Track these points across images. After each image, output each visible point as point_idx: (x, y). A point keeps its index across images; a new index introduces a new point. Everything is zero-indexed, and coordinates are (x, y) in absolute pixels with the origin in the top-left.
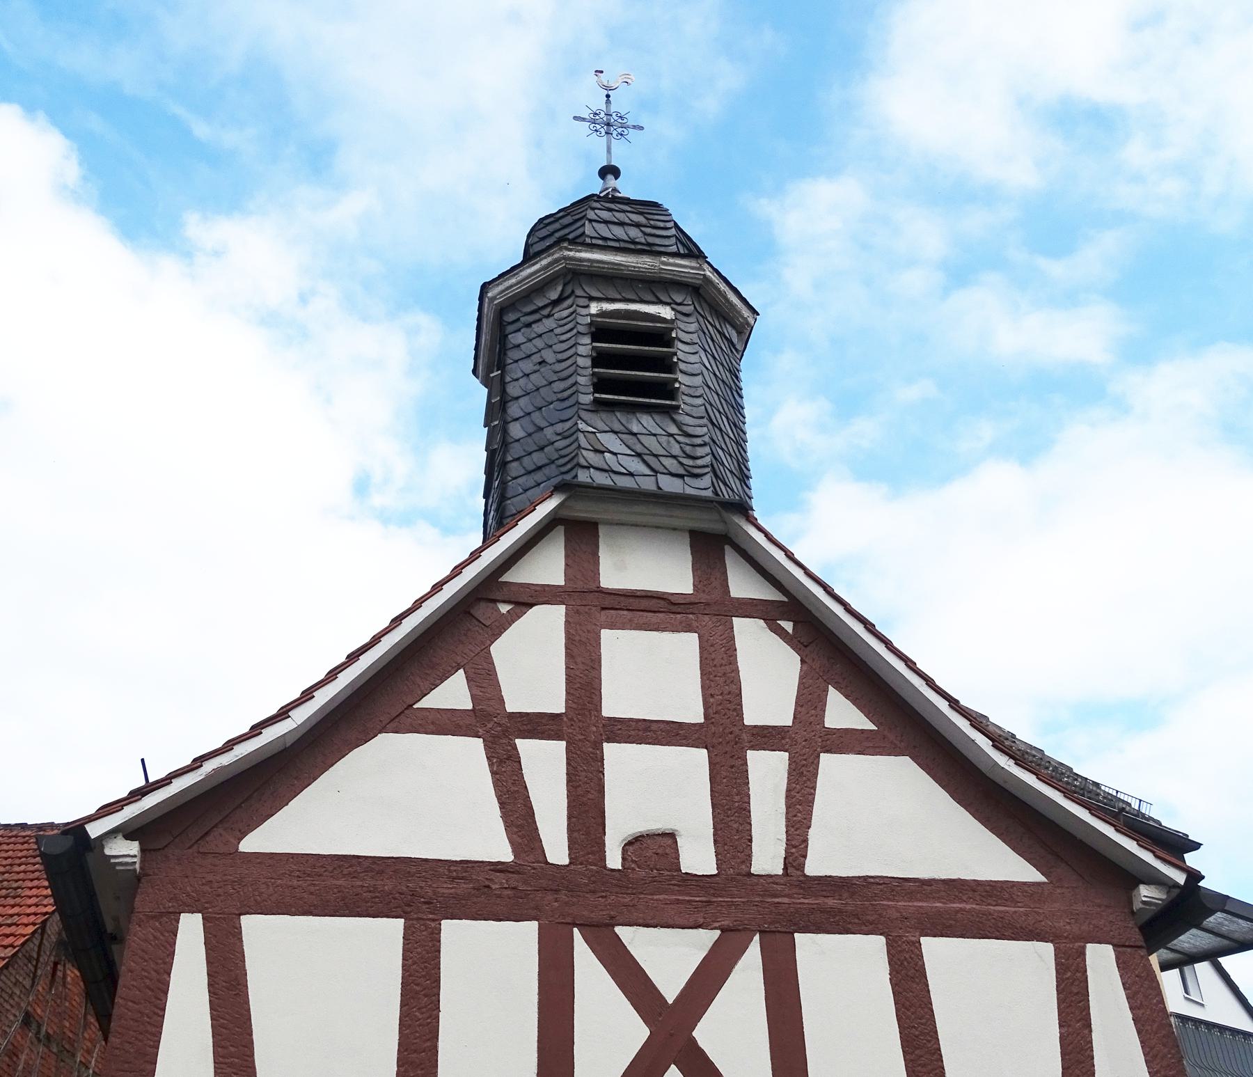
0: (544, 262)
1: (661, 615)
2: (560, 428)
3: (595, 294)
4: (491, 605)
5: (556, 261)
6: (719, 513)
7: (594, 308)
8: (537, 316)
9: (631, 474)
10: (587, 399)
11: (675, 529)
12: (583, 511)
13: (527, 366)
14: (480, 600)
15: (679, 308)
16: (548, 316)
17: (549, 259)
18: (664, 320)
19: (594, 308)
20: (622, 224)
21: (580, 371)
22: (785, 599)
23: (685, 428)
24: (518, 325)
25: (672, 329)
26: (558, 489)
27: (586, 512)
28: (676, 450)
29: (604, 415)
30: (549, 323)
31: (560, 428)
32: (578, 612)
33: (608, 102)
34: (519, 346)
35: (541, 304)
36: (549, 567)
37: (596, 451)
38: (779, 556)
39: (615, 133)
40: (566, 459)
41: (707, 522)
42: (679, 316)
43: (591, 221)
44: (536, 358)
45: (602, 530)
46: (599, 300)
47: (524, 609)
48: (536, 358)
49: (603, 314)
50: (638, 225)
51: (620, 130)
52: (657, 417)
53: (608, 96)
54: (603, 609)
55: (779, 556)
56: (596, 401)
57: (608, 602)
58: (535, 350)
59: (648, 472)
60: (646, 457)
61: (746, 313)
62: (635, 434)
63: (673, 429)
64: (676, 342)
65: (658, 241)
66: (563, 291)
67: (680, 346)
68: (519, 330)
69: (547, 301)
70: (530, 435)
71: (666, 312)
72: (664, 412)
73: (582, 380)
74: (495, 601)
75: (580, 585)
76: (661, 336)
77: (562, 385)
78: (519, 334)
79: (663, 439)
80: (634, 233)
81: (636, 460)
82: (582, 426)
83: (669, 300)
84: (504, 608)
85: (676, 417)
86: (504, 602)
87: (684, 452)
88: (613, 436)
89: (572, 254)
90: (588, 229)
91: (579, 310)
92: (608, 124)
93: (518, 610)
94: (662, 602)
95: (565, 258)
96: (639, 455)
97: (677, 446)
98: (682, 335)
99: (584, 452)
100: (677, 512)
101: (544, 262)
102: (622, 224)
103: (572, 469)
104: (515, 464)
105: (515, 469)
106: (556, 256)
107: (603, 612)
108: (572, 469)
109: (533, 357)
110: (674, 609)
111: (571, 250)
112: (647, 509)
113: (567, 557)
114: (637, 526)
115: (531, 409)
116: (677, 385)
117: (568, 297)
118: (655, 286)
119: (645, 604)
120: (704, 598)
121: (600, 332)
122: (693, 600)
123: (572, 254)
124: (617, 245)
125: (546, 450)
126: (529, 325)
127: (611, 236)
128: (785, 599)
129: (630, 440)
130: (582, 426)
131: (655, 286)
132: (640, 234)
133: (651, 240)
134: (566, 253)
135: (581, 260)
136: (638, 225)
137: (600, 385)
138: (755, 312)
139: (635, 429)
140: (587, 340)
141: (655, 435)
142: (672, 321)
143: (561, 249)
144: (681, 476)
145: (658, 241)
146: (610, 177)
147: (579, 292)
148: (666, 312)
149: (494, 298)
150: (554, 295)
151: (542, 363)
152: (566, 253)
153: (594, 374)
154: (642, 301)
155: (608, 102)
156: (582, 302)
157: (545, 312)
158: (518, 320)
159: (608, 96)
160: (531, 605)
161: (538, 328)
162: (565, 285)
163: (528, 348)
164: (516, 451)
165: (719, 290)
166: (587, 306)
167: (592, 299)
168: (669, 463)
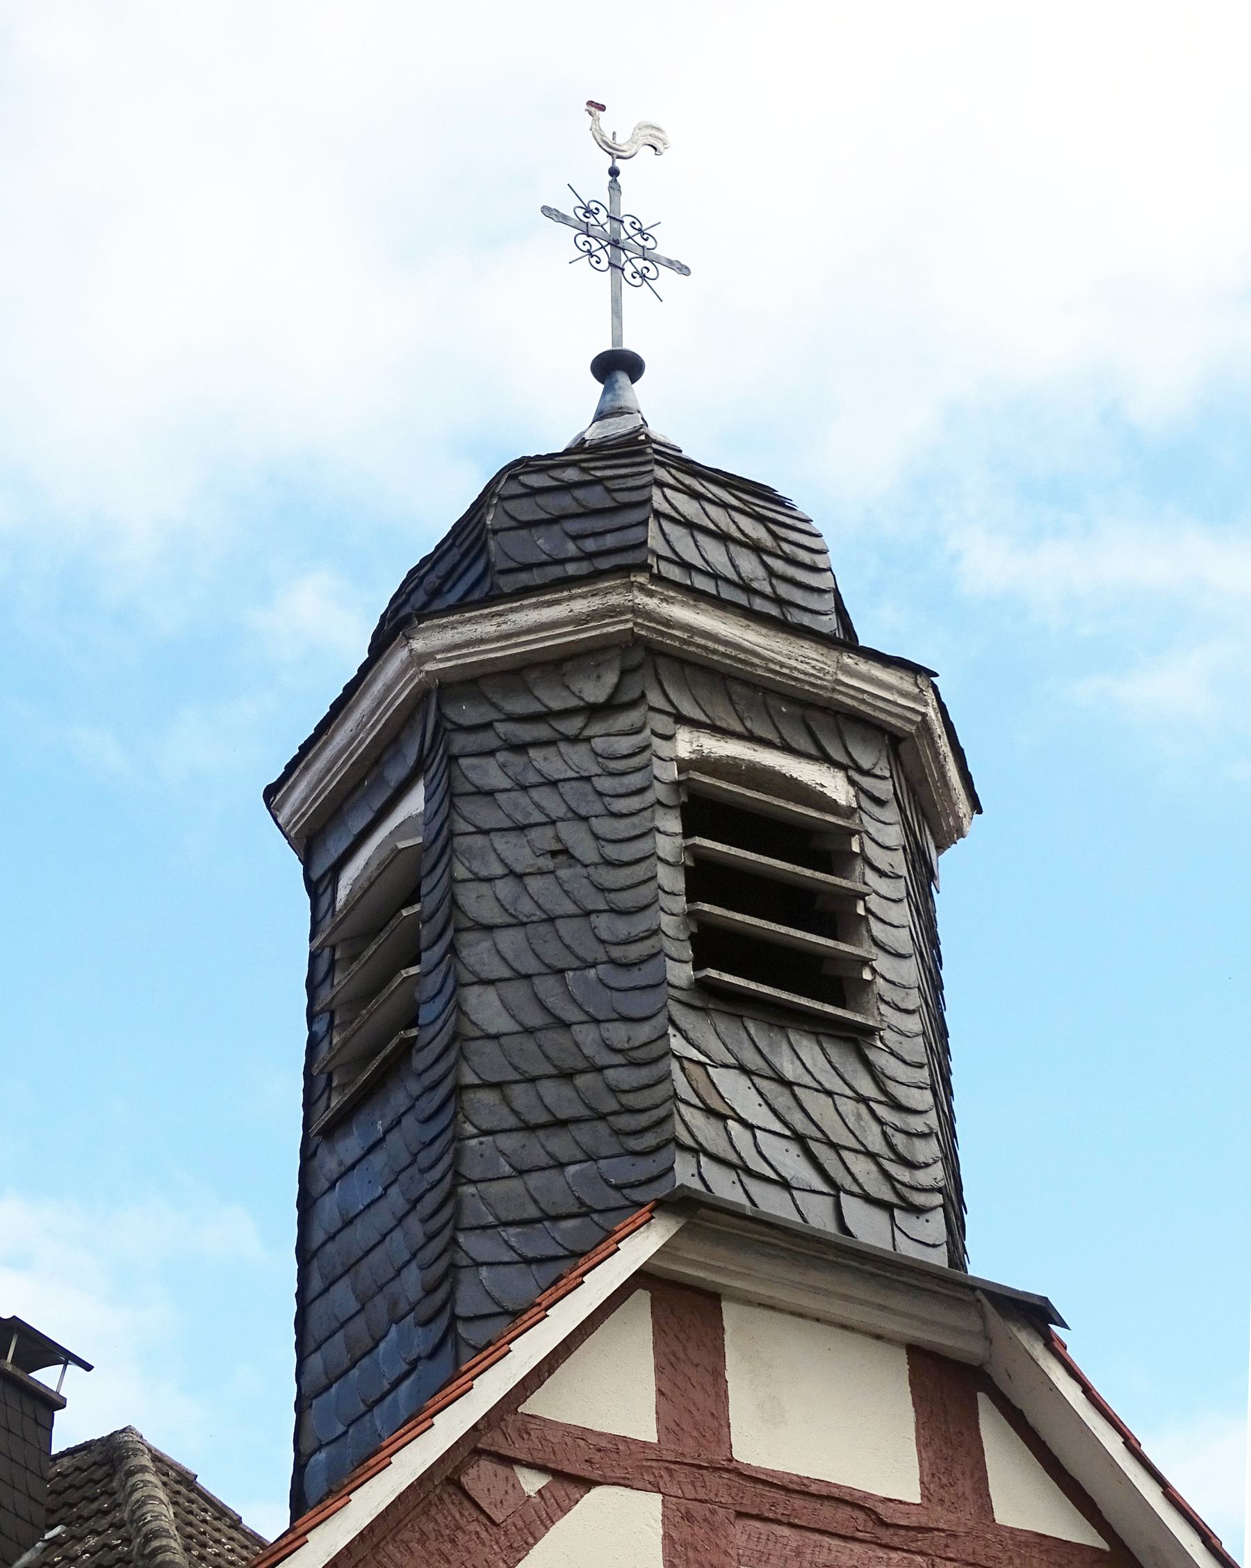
0: (581, 606)
1: (857, 1548)
2: (618, 1034)
3: (689, 709)
4: (502, 1471)
5: (613, 612)
6: (983, 1316)
7: (686, 744)
8: (540, 731)
9: (785, 1184)
10: (681, 973)
11: (878, 1337)
12: (701, 1265)
13: (518, 852)
14: (478, 1453)
15: (866, 782)
16: (574, 740)
17: (595, 603)
18: (830, 806)
19: (686, 744)
20: (723, 537)
21: (665, 901)
22: (1105, 1546)
23: (892, 1088)
24: (486, 740)
25: (853, 833)
26: (664, 1206)
27: (704, 1266)
28: (875, 1142)
29: (722, 1024)
30: (579, 757)
31: (618, 1034)
32: (688, 1517)
33: (614, 188)
34: (490, 793)
35: (556, 705)
36: (618, 1395)
37: (710, 1112)
38: (1112, 1444)
39: (629, 269)
40: (644, 1120)
41: (951, 1334)
42: (866, 804)
43: (658, 514)
44: (543, 838)
45: (731, 1314)
46: (695, 724)
47: (574, 1492)
48: (543, 838)
49: (702, 763)
50: (756, 548)
51: (640, 264)
52: (832, 1050)
53: (614, 172)
54: (740, 1515)
55: (1112, 1444)
56: (704, 987)
57: (751, 1499)
58: (538, 817)
59: (819, 1184)
60: (814, 1146)
61: (963, 807)
62: (788, 1085)
63: (867, 1087)
64: (859, 866)
65: (797, 596)
66: (617, 688)
67: (871, 877)
68: (492, 753)
69: (574, 702)
70: (529, 1031)
71: (836, 787)
72: (846, 1040)
73: (667, 923)
74: (510, 1461)
75: (689, 1449)
76: (824, 843)
77: (624, 928)
78: (490, 764)
79: (848, 1107)
80: (749, 565)
81: (794, 1149)
82: (677, 1043)
83: (843, 759)
84: (532, 1483)
85: (872, 1055)
86: (531, 1466)
87: (891, 1146)
88: (744, 1081)
89: (652, 603)
90: (655, 542)
91: (656, 742)
92: (615, 244)
93: (561, 1491)
94: (861, 1516)
95: (635, 610)
96: (800, 1139)
97: (876, 1129)
98: (872, 851)
99: (682, 1107)
100: (898, 1301)
101: (581, 606)
102: (723, 537)
103: (657, 1149)
104: (488, 1097)
105: (485, 1107)
106: (614, 599)
107: (740, 1524)
108: (657, 1149)
109: (534, 834)
110: (886, 1536)
111: (651, 594)
112: (833, 1274)
113: (659, 1369)
114: (801, 1316)
115: (529, 965)
116: (867, 975)
117: (632, 705)
118: (822, 720)
119: (827, 1515)
120: (941, 1518)
121: (702, 808)
122: (924, 1521)
123: (652, 603)
124: (742, 599)
125: (580, 1081)
126: (520, 748)
127: (699, 563)
128: (1105, 1546)
129: (782, 1099)
130: (677, 1043)
131: (822, 720)
132: (761, 572)
133: (784, 590)
134: (641, 599)
135: (668, 623)
136: (756, 548)
137: (710, 944)
138: (976, 807)
139: (790, 1070)
140: (672, 823)
141: (830, 1094)
142: (849, 812)
143: (630, 586)
144: (886, 1206)
145: (797, 596)
146: (623, 378)
147: (655, 699)
148: (836, 787)
149: (420, 659)
150: (595, 691)
151: (563, 853)
152: (641, 599)
153: (690, 914)
154: (787, 748)
155: (614, 188)
156: (662, 723)
157: (571, 726)
158: (488, 726)
159: (614, 172)
160: (588, 1484)
161: (549, 763)
162: (624, 673)
163: (521, 807)
164: (486, 1062)
165: (936, 753)
166: (669, 738)
167: (681, 719)
168: (861, 1166)
